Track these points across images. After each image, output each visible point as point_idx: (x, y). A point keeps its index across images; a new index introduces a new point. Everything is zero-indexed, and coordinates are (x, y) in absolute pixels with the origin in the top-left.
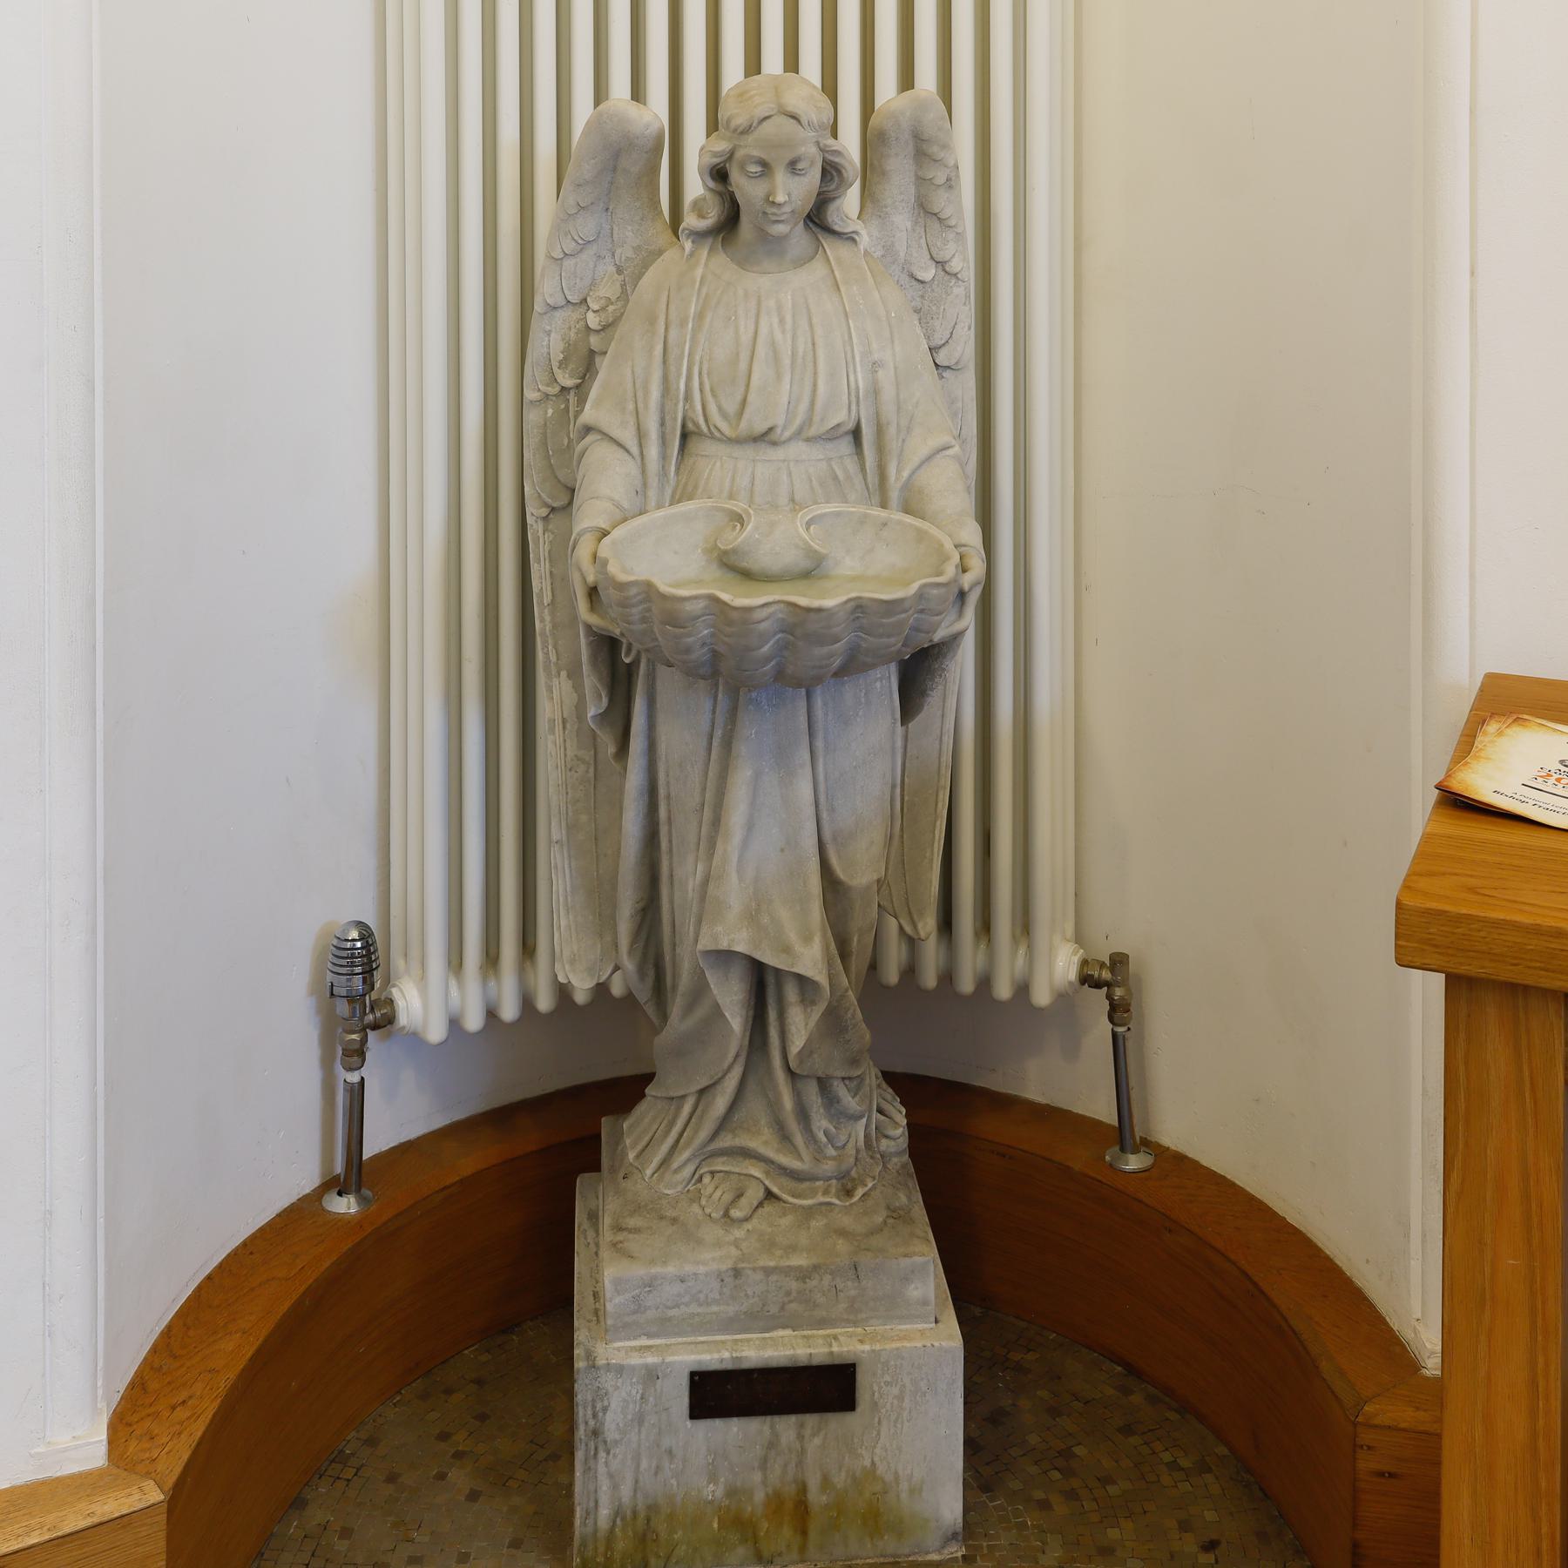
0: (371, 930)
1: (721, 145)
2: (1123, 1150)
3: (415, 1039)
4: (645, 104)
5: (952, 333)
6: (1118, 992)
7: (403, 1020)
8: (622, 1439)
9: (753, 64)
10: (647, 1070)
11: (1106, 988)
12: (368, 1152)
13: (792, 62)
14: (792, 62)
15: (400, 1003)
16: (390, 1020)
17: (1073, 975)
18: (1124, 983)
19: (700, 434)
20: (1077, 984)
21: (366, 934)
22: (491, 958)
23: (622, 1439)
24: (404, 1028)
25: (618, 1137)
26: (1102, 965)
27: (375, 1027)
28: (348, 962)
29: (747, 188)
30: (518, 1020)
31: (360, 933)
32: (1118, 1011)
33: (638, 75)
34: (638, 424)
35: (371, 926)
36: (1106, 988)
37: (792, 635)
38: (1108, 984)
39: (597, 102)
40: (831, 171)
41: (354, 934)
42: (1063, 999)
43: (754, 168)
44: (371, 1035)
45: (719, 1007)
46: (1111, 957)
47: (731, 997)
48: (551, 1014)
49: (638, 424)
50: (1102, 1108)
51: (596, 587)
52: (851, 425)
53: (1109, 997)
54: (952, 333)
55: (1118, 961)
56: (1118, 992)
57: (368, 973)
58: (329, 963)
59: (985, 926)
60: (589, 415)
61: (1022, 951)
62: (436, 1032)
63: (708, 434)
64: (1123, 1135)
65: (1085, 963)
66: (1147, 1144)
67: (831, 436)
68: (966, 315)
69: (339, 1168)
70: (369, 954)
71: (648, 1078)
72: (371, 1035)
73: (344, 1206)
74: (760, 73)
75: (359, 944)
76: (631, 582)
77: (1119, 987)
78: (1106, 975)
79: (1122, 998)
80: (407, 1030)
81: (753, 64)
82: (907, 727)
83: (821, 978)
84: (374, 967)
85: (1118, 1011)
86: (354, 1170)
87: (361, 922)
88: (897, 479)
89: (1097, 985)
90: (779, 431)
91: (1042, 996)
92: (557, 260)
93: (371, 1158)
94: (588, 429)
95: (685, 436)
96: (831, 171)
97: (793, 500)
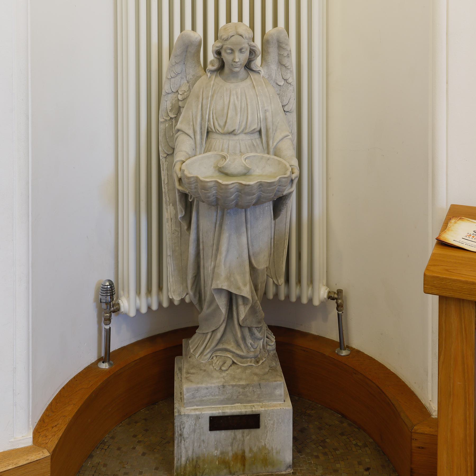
0: (113, 282)
1: (219, 44)
2: (341, 349)
3: (126, 315)
4: (196, 32)
5: (289, 101)
6: (340, 301)
7: (122, 309)
8: (189, 437)
9: (229, 19)
10: (197, 325)
11: (336, 300)
12: (112, 350)
13: (240, 19)
14: (240, 19)
15: (121, 305)
16: (118, 310)
17: (326, 296)
18: (341, 298)
19: (212, 132)
20: (327, 299)
21: (111, 284)
22: (149, 291)
23: (189, 437)
24: (123, 312)
25: (188, 345)
26: (335, 293)
27: (114, 312)
28: (106, 292)
29: (227, 57)
30: (157, 310)
31: (109, 283)
32: (339, 307)
33: (194, 23)
34: (194, 129)
35: (113, 281)
36: (336, 300)
37: (240, 193)
38: (336, 299)
39: (181, 31)
40: (252, 52)
41: (108, 284)
42: (323, 303)
43: (229, 51)
44: (113, 314)
45: (218, 306)
46: (337, 290)
47: (222, 303)
48: (167, 308)
49: (194, 129)
50: (335, 336)
51: (181, 178)
52: (258, 129)
53: (337, 303)
54: (289, 101)
55: (340, 292)
56: (340, 301)
57: (112, 295)
58: (100, 292)
59: (299, 281)
60: (179, 126)
61: (310, 289)
62: (132, 313)
63: (215, 132)
64: (341, 344)
65: (329, 292)
66: (348, 347)
67: (252, 132)
68: (293, 96)
69: (103, 354)
70: (112, 290)
71: (197, 327)
72: (113, 314)
73: (105, 366)
74: (231, 22)
75: (109, 287)
76: (192, 177)
77: (340, 299)
78: (336, 296)
79: (341, 303)
80: (123, 313)
81: (229, 19)
82: (275, 221)
83: (249, 297)
84: (114, 293)
85: (339, 307)
86: (108, 355)
87: (110, 280)
88: (272, 145)
89: (333, 299)
90: (236, 131)
91: (316, 302)
92: (169, 79)
93: (113, 352)
94: (178, 130)
95: (208, 132)
96: (252, 52)
97: (241, 152)
